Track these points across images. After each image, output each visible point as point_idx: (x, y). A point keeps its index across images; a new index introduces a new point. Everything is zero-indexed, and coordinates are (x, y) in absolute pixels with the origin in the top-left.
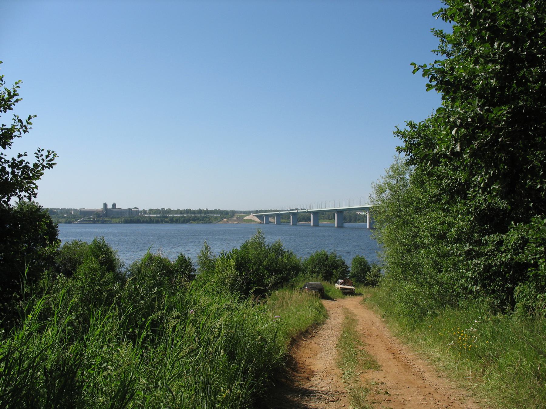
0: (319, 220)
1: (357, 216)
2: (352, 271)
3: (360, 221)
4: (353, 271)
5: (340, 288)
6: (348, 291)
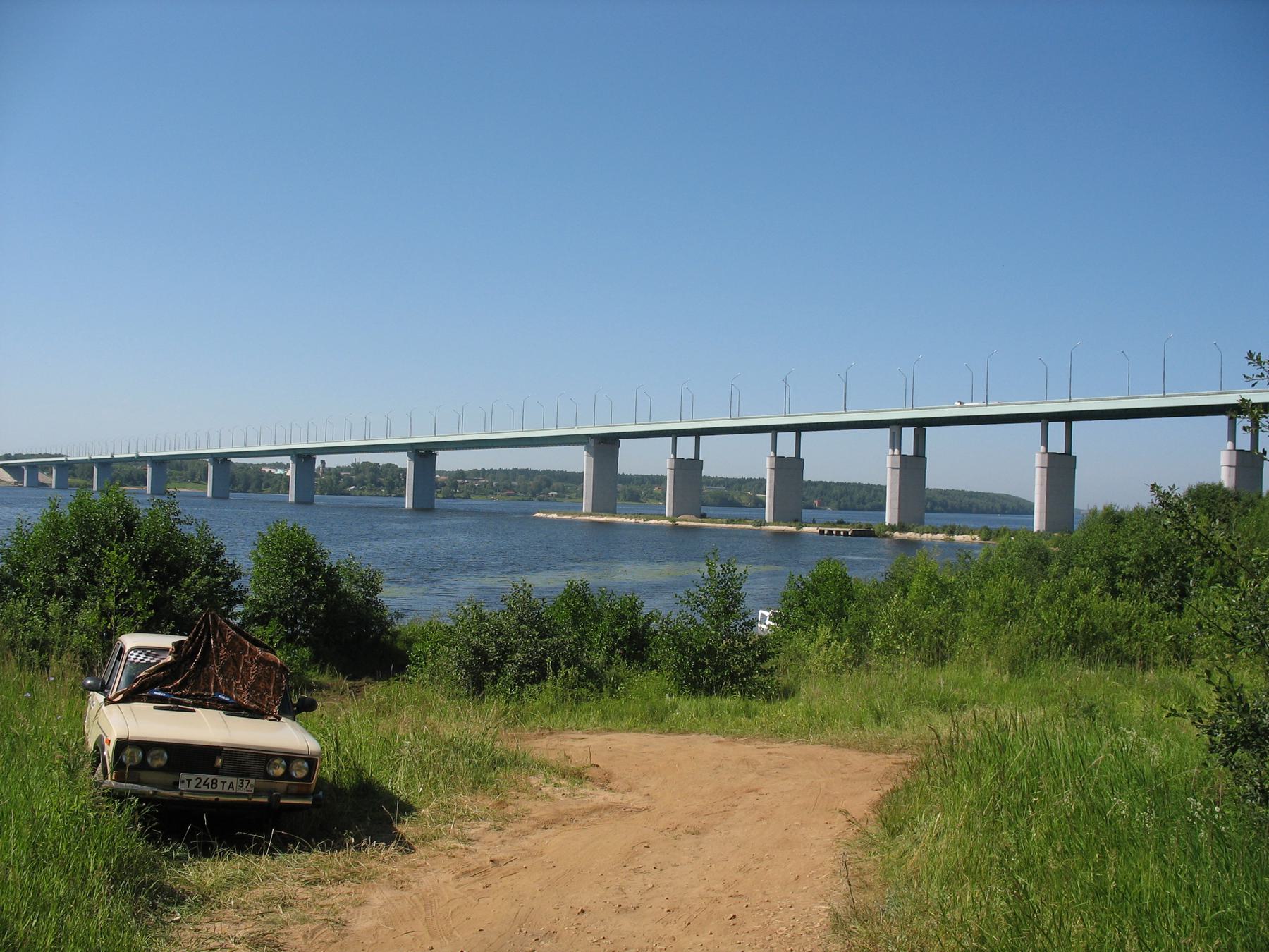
0: (168, 482)
1: (263, 476)
2: (251, 595)
3: (269, 489)
4: (257, 590)
5: (121, 745)
6: (229, 788)
